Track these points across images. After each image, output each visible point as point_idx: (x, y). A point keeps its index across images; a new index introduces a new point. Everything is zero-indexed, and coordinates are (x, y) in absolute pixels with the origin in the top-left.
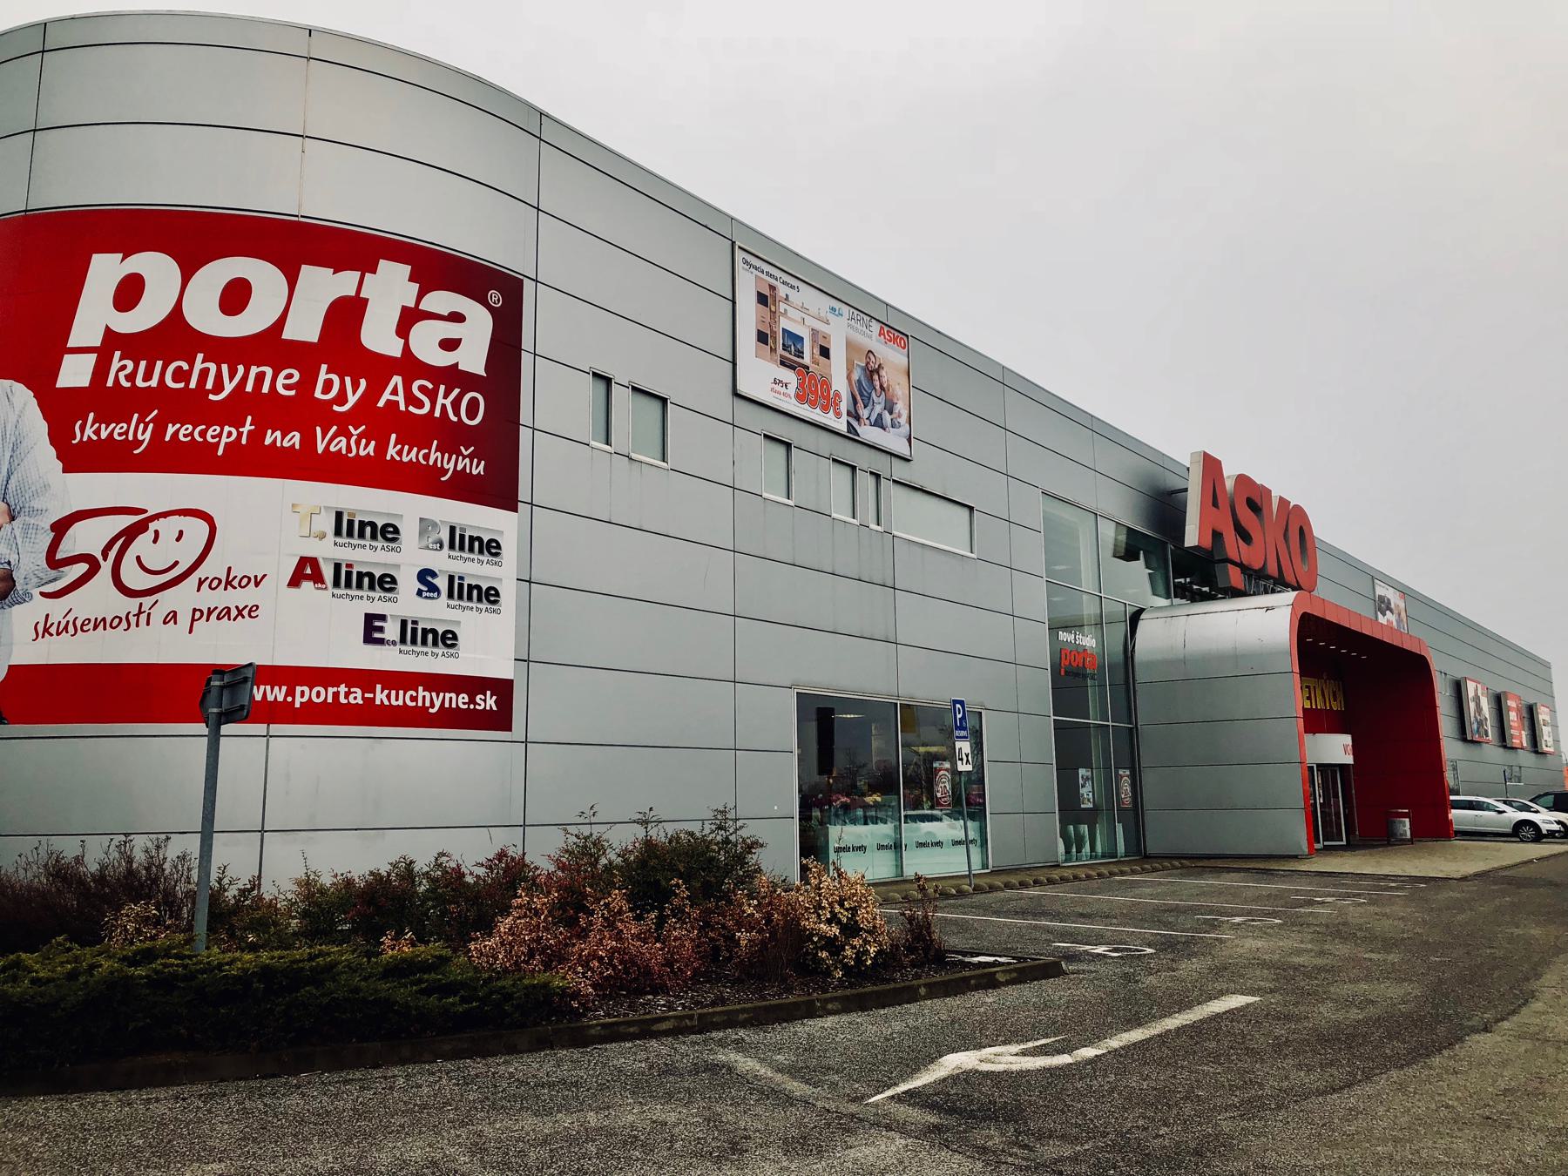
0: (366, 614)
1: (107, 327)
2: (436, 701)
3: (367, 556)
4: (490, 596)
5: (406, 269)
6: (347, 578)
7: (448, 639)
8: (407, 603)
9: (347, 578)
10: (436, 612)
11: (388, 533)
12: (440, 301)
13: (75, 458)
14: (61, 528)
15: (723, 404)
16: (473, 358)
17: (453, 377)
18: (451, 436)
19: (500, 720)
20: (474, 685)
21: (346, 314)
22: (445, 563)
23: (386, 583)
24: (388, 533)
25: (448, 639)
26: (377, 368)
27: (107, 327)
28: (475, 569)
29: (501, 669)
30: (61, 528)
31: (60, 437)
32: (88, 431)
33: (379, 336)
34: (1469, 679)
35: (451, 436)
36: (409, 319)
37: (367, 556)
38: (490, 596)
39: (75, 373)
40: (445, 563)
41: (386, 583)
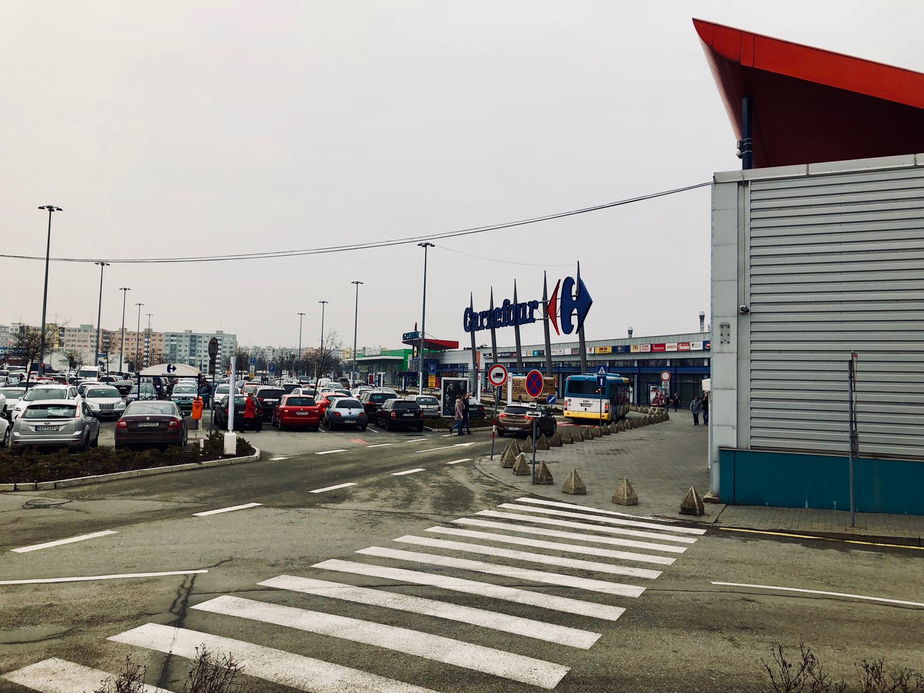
0: (458, 342)
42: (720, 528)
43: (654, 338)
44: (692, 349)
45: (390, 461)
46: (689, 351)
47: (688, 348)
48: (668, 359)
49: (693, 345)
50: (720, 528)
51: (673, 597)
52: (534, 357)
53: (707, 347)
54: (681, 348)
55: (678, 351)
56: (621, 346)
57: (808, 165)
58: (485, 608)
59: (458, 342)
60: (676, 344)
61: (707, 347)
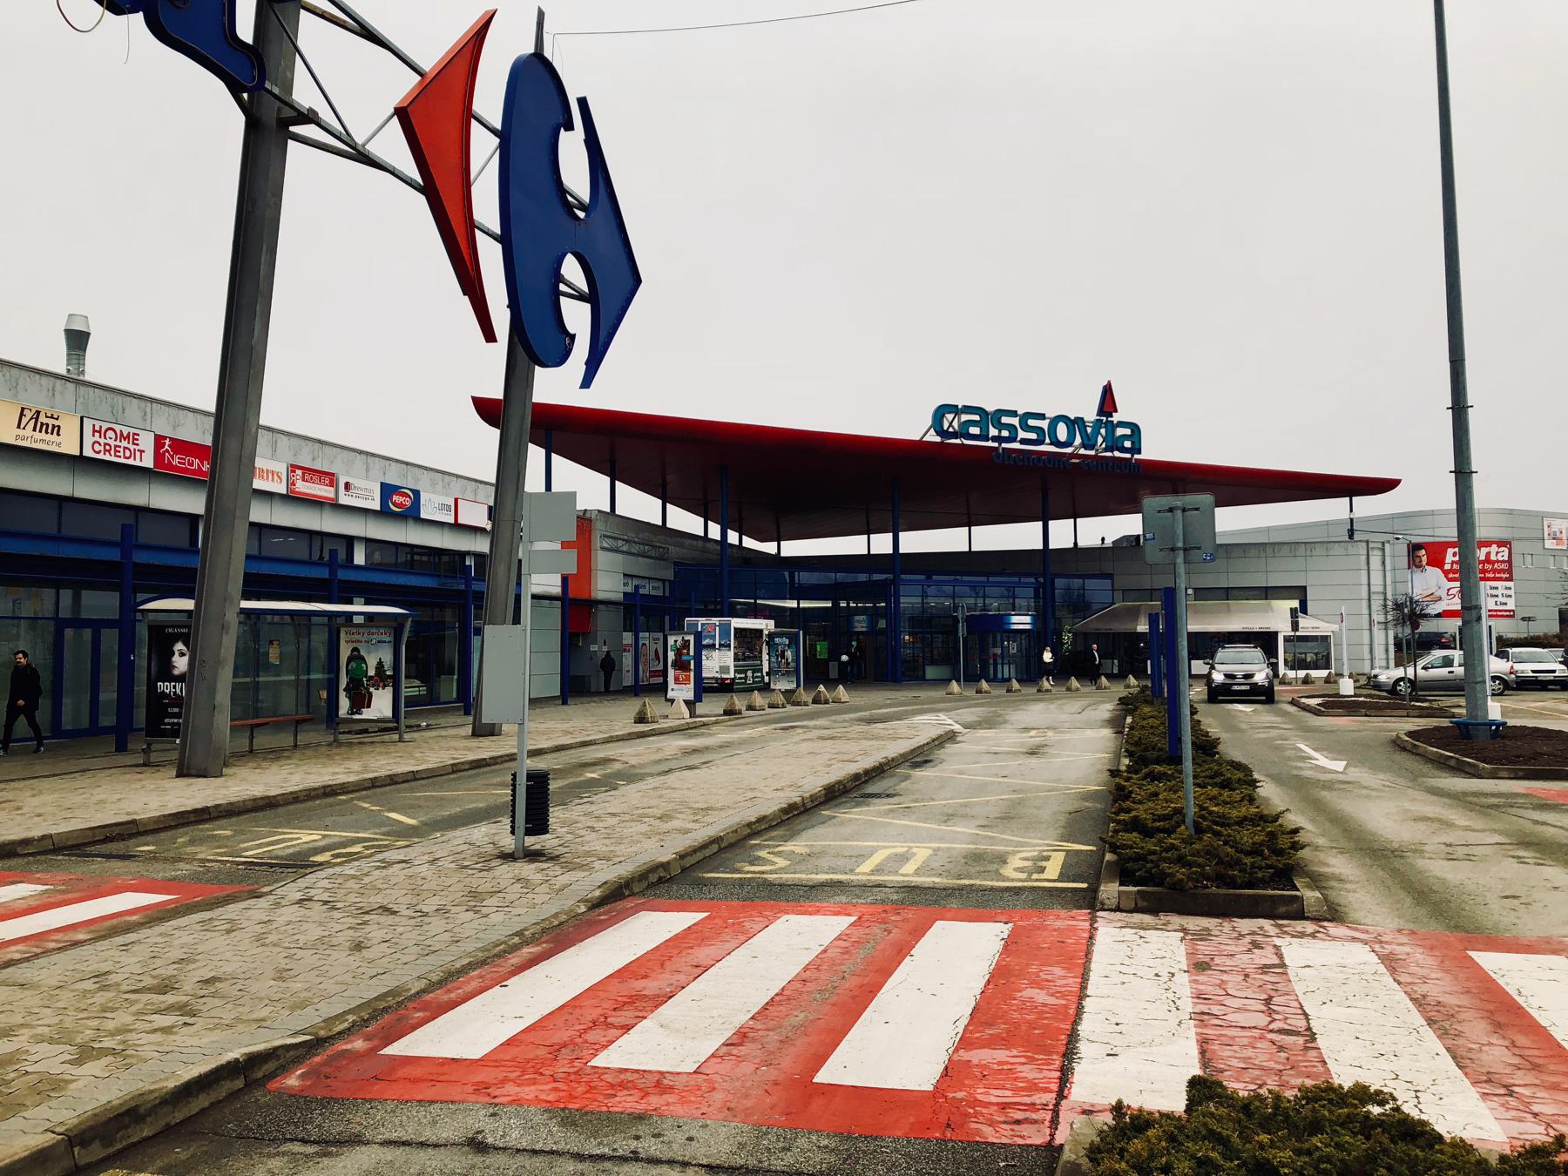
0: (574, 494)
1: (581, 388)
2: (1505, 614)
3: (1494, 592)
4: (1510, 596)
5: (1152, 450)
6: (1492, 596)
7: (1506, 604)
8: (1500, 599)
9: (1492, 596)
10: (1504, 600)
11: (1497, 588)
12: (1501, 549)
13: (1450, 580)
14: (1448, 590)
15: (1542, 552)
16: (1506, 558)
17: (1503, 562)
18: (1503, 571)
19: (1513, 616)
20: (1510, 611)
21: (1488, 554)
22: (1505, 592)
23: (1497, 596)
24: (1497, 588)
25: (1506, 604)
26: (1493, 563)
27: (581, 388)
28: (1509, 592)
29: (1513, 608)
30: (1448, 590)
31: (1446, 577)
32: (1451, 576)
33: (1493, 557)
34: (820, 1059)
35: (1503, 571)
36: (1497, 553)
37: (1494, 592)
38: (1510, 596)
39: (1447, 567)
40: (1505, 592)
41: (1497, 596)
42: (1264, 698)
43: (302, 442)
44: (344, 500)
45: (544, 945)
46: (336, 506)
47: (332, 495)
48: (360, 539)
49: (347, 486)
50: (1264, 698)
51: (1151, 1133)
52: (161, 473)
53: (395, 504)
54: (303, 487)
55: (1355, 696)
56: (171, 439)
57: (1076, 543)
58: (1440, 103)
59: (574, 494)
60: (282, 469)
61: (395, 504)
